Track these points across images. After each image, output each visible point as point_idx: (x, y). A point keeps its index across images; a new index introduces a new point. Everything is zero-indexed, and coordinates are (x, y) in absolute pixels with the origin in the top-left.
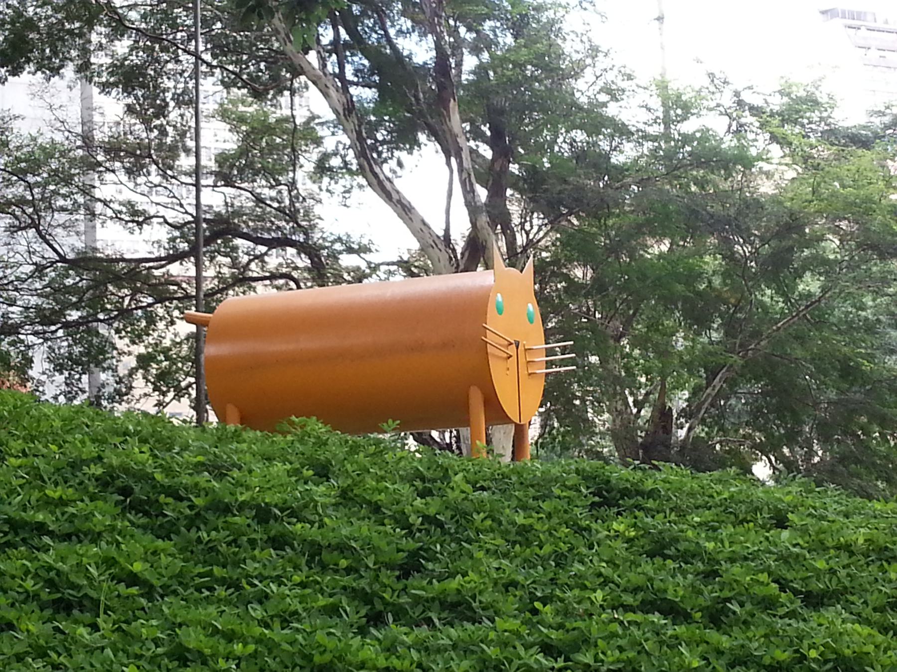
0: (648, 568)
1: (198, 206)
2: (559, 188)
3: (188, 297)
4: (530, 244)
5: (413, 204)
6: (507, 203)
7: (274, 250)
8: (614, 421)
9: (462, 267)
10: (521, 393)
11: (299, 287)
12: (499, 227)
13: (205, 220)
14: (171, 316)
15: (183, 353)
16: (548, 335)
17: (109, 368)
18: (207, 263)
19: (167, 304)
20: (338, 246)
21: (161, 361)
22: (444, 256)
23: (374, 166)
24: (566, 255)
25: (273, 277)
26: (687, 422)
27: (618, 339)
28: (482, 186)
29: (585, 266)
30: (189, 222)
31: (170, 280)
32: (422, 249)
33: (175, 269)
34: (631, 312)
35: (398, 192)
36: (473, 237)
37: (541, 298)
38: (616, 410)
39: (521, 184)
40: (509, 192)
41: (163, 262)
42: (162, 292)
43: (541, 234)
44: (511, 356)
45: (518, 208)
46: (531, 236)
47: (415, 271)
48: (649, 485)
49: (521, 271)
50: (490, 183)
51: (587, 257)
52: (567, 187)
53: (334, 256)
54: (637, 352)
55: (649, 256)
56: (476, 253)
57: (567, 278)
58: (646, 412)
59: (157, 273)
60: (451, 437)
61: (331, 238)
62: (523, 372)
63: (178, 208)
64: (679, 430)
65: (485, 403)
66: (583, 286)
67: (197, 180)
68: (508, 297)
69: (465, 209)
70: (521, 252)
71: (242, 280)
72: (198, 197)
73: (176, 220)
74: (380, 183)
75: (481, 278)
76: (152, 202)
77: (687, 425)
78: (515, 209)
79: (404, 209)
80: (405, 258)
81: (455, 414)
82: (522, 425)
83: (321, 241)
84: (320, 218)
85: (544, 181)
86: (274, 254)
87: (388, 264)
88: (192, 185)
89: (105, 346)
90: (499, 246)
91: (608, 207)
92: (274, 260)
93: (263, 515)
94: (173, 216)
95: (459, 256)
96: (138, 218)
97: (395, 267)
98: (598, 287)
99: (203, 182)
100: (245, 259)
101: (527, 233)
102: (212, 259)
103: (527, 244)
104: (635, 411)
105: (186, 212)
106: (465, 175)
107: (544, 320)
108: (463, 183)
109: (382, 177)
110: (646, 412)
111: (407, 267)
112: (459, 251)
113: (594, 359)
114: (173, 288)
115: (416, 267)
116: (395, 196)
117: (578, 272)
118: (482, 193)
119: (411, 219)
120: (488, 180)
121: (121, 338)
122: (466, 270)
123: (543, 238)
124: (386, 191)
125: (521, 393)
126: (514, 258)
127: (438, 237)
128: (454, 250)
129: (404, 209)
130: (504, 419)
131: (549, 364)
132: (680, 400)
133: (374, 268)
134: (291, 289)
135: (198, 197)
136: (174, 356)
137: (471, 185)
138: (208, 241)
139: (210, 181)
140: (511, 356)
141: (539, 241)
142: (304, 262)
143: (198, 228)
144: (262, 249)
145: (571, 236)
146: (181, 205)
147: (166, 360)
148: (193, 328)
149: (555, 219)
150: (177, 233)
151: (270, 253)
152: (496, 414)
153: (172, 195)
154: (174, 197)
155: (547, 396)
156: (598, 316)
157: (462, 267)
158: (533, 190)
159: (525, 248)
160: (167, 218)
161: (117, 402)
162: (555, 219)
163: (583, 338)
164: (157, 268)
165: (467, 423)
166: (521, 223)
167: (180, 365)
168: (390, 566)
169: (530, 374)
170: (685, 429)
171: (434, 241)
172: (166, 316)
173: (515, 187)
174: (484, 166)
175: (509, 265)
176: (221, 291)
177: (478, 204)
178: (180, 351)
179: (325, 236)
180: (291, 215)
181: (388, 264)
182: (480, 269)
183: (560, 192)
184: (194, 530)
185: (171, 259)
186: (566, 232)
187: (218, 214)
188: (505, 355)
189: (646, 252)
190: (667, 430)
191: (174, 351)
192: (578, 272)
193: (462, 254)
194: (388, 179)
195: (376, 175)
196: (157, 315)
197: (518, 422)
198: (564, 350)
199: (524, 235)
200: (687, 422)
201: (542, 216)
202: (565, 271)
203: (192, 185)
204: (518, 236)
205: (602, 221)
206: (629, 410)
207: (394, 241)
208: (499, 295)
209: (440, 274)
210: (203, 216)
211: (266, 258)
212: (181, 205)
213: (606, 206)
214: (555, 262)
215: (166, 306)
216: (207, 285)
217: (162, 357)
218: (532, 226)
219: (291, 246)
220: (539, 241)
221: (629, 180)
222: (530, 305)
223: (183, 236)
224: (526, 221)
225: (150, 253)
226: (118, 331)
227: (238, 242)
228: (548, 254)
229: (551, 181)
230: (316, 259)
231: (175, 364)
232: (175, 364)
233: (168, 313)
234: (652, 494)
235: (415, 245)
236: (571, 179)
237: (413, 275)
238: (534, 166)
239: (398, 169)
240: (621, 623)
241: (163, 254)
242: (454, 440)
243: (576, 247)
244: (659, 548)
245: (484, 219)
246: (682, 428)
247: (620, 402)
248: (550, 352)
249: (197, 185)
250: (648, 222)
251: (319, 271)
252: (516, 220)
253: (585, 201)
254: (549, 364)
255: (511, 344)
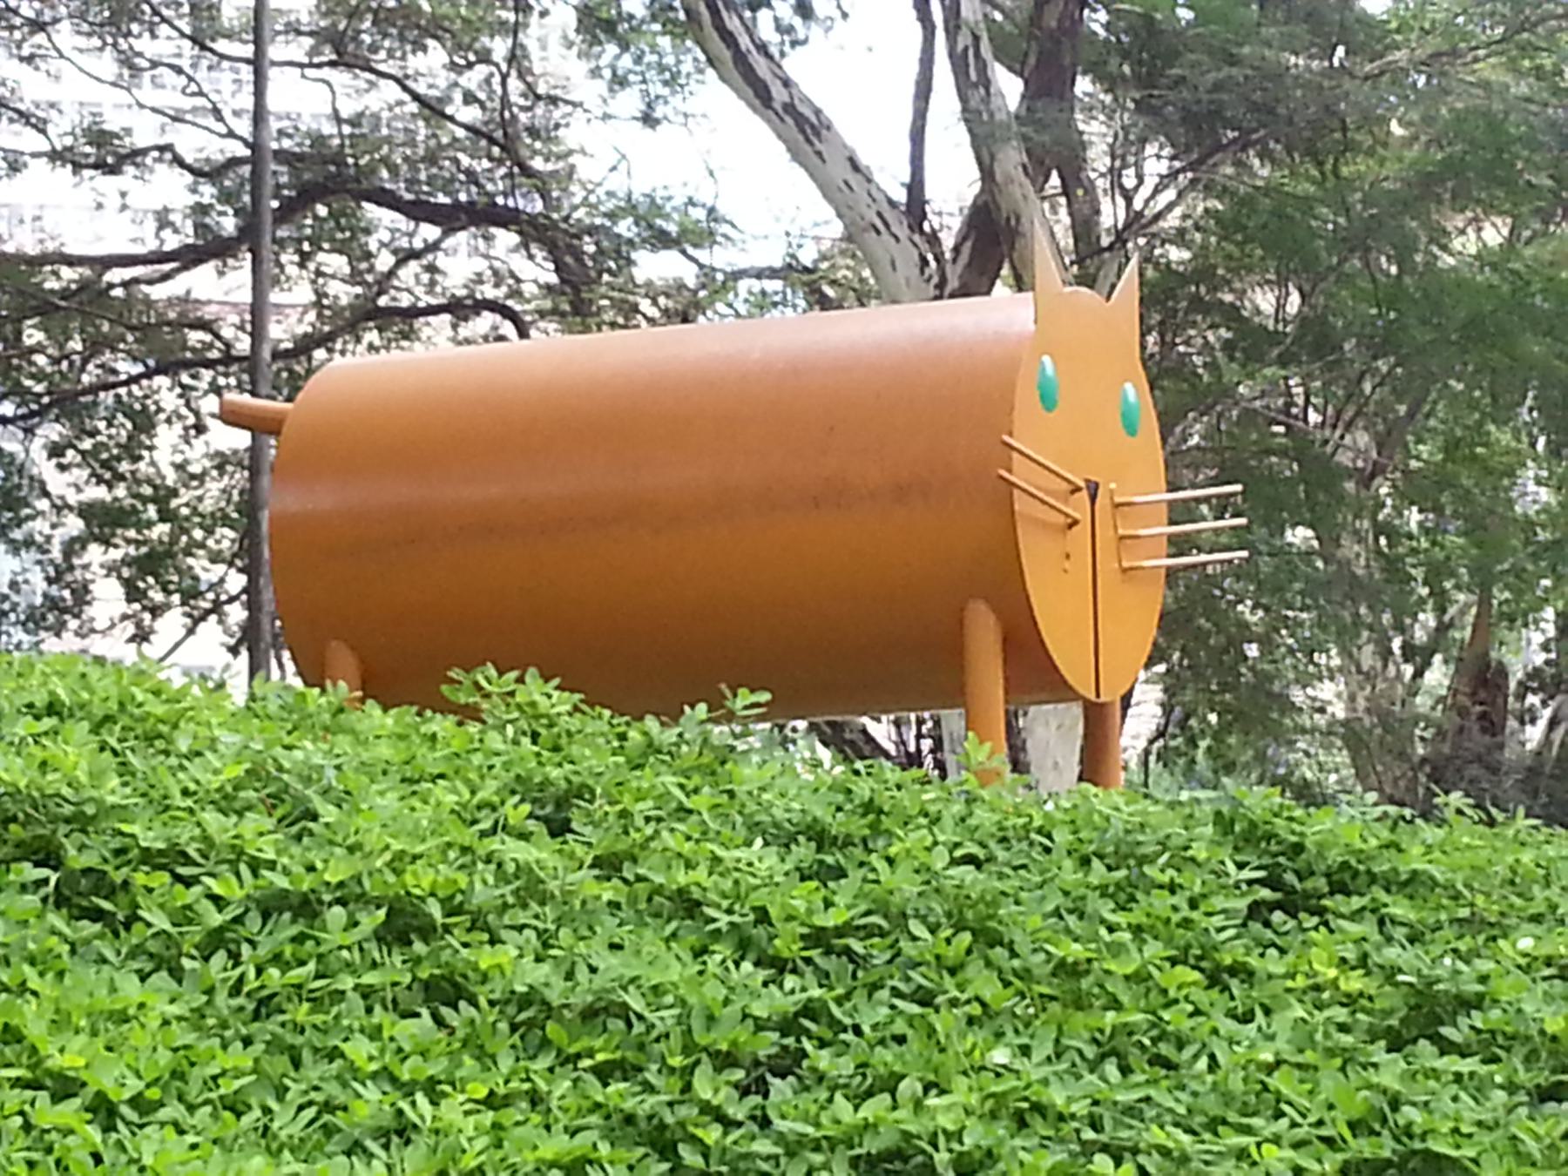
0: (1390, 1071)
1: (259, 116)
2: (1212, 77)
3: (228, 359)
4: (1135, 222)
5: (829, 112)
6: (1078, 116)
7: (462, 236)
8: (1352, 698)
9: (953, 284)
10: (1099, 611)
11: (523, 333)
12: (1055, 180)
13: (280, 155)
14: (197, 414)
15: (207, 506)
16: (1178, 466)
17: (29, 543)
18: (292, 270)
19: (185, 378)
20: (625, 228)
21: (150, 524)
22: (906, 256)
23: (724, 14)
24: (1229, 257)
25: (460, 309)
26: (1544, 704)
27: (1366, 479)
28: (1010, 69)
29: (1281, 283)
30: (234, 162)
31: (190, 316)
32: (849, 238)
33: (202, 282)
34: (1402, 409)
35: (787, 83)
36: (986, 204)
37: (1162, 372)
38: (1359, 671)
39: (1114, 62)
40: (1083, 85)
41: (167, 267)
42: (170, 345)
43: (1169, 195)
44: (1075, 522)
45: (1104, 129)
46: (1138, 204)
47: (830, 291)
48: (1414, 859)
49: (1108, 298)
50: (1032, 60)
51: (1290, 256)
52: (1234, 71)
53: (621, 252)
54: (1414, 517)
55: (1451, 261)
56: (991, 247)
57: (1232, 315)
58: (1438, 676)
59: (158, 292)
60: (919, 736)
61: (610, 205)
62: (1107, 565)
63: (210, 121)
64: (1528, 728)
65: (1005, 640)
66: (1275, 337)
67: (258, 43)
68: (1060, 363)
69: (962, 127)
70: (1111, 248)
71: (379, 315)
72: (259, 93)
73: (203, 155)
74: (740, 58)
75: (1002, 311)
76: (141, 106)
77: (1547, 713)
78: (1097, 133)
79: (804, 130)
80: (807, 257)
81: (918, 667)
82: (1103, 705)
83: (580, 213)
84: (583, 152)
85: (1172, 57)
86: (463, 250)
87: (759, 274)
88: (247, 61)
89: (19, 487)
90: (1049, 226)
91: (1344, 129)
92: (462, 261)
93: (403, 925)
94: (197, 144)
95: (948, 256)
96: (103, 153)
97: (777, 285)
98: (1313, 342)
99: (275, 51)
100: (385, 261)
101: (1128, 197)
102: (304, 259)
103: (1127, 226)
104: (1408, 670)
105: (231, 134)
106: (964, 40)
107: (1168, 422)
108: (959, 63)
109: (744, 42)
110: (1438, 676)
111: (812, 286)
112: (948, 241)
113: (1299, 536)
114: (195, 337)
115: (833, 283)
116: (779, 94)
117: (1265, 301)
118: (1009, 87)
119: (819, 154)
120: (1026, 55)
121: (62, 468)
122: (964, 292)
123: (1170, 207)
124: (760, 88)
125: (1099, 611)
126: (1090, 259)
127: (892, 204)
128: (933, 239)
129: (804, 130)
130: (1056, 688)
131: (1179, 545)
132: (1528, 649)
133: (718, 285)
134: (501, 338)
135: (259, 93)
136: (185, 511)
137: (982, 68)
138: (287, 213)
139: (299, 49)
140: (1075, 522)
141: (1158, 216)
142: (536, 271)
143: (256, 178)
144: (430, 232)
145: (1247, 203)
146: (217, 113)
147: (162, 520)
148: (240, 439)
149: (1201, 161)
150: (208, 192)
151: (448, 243)
152: (1033, 672)
153: (193, 88)
154: (201, 94)
155: (1169, 622)
156: (1314, 417)
157: (953, 284)
158: (1146, 80)
159: (1120, 238)
160: (179, 149)
161: (47, 629)
162: (1201, 161)
163: (1273, 478)
164: (150, 282)
165: (955, 693)
166: (1111, 170)
167: (198, 534)
168: (724, 1061)
169: (1125, 571)
170: (1542, 724)
171: (879, 215)
172: (184, 411)
173: (1097, 71)
174: (1018, 17)
175: (1082, 280)
176: (325, 340)
177: (1000, 116)
178: (200, 499)
179: (593, 199)
180: (503, 138)
181: (759, 274)
182: (1001, 290)
183: (1218, 87)
184: (220, 958)
185: (189, 257)
186: (1233, 194)
187: (319, 140)
188: (1062, 519)
189: (1444, 248)
190: (1492, 725)
191: (185, 496)
192: (1265, 301)
193: (957, 249)
194: (763, 48)
195: (728, 38)
196: (160, 410)
197: (1092, 697)
198: (1221, 507)
199: (1120, 201)
200: (1544, 704)
201: (1167, 151)
202: (1228, 298)
203: (247, 61)
204: (1106, 205)
205: (1328, 167)
206: (1392, 670)
207: (773, 209)
208: (1046, 359)
209: (894, 302)
210: (274, 145)
211: (441, 260)
212: (220, 119)
213: (1336, 124)
214: (1202, 272)
215: (183, 386)
216: (280, 332)
217: (152, 511)
218: (1140, 179)
219: (504, 225)
220: (1158, 216)
221: (1400, 56)
222: (1129, 388)
223: (226, 197)
224: (1125, 166)
225: (134, 240)
226: (55, 451)
227: (371, 210)
228: (1186, 255)
229: (1193, 57)
230: (569, 259)
231: (187, 532)
232: (187, 532)
233: (188, 405)
234: (1412, 885)
235: (837, 228)
236: (1246, 50)
237: (825, 303)
238: (1148, 19)
239: (797, 22)
240: (283, 677)
241: (172, 242)
242: (927, 744)
243: (1261, 232)
244: (1425, 1018)
245: (1011, 158)
246: (1533, 721)
247: (1370, 648)
248: (1179, 512)
249: (258, 64)
250: (1452, 167)
251: (577, 291)
252: (1098, 159)
253: (1282, 110)
254: (1179, 545)
255: (1078, 489)
